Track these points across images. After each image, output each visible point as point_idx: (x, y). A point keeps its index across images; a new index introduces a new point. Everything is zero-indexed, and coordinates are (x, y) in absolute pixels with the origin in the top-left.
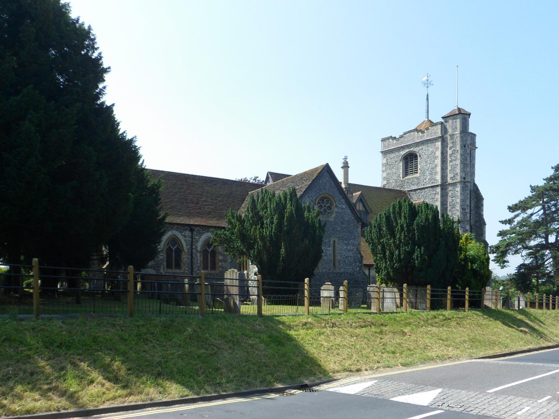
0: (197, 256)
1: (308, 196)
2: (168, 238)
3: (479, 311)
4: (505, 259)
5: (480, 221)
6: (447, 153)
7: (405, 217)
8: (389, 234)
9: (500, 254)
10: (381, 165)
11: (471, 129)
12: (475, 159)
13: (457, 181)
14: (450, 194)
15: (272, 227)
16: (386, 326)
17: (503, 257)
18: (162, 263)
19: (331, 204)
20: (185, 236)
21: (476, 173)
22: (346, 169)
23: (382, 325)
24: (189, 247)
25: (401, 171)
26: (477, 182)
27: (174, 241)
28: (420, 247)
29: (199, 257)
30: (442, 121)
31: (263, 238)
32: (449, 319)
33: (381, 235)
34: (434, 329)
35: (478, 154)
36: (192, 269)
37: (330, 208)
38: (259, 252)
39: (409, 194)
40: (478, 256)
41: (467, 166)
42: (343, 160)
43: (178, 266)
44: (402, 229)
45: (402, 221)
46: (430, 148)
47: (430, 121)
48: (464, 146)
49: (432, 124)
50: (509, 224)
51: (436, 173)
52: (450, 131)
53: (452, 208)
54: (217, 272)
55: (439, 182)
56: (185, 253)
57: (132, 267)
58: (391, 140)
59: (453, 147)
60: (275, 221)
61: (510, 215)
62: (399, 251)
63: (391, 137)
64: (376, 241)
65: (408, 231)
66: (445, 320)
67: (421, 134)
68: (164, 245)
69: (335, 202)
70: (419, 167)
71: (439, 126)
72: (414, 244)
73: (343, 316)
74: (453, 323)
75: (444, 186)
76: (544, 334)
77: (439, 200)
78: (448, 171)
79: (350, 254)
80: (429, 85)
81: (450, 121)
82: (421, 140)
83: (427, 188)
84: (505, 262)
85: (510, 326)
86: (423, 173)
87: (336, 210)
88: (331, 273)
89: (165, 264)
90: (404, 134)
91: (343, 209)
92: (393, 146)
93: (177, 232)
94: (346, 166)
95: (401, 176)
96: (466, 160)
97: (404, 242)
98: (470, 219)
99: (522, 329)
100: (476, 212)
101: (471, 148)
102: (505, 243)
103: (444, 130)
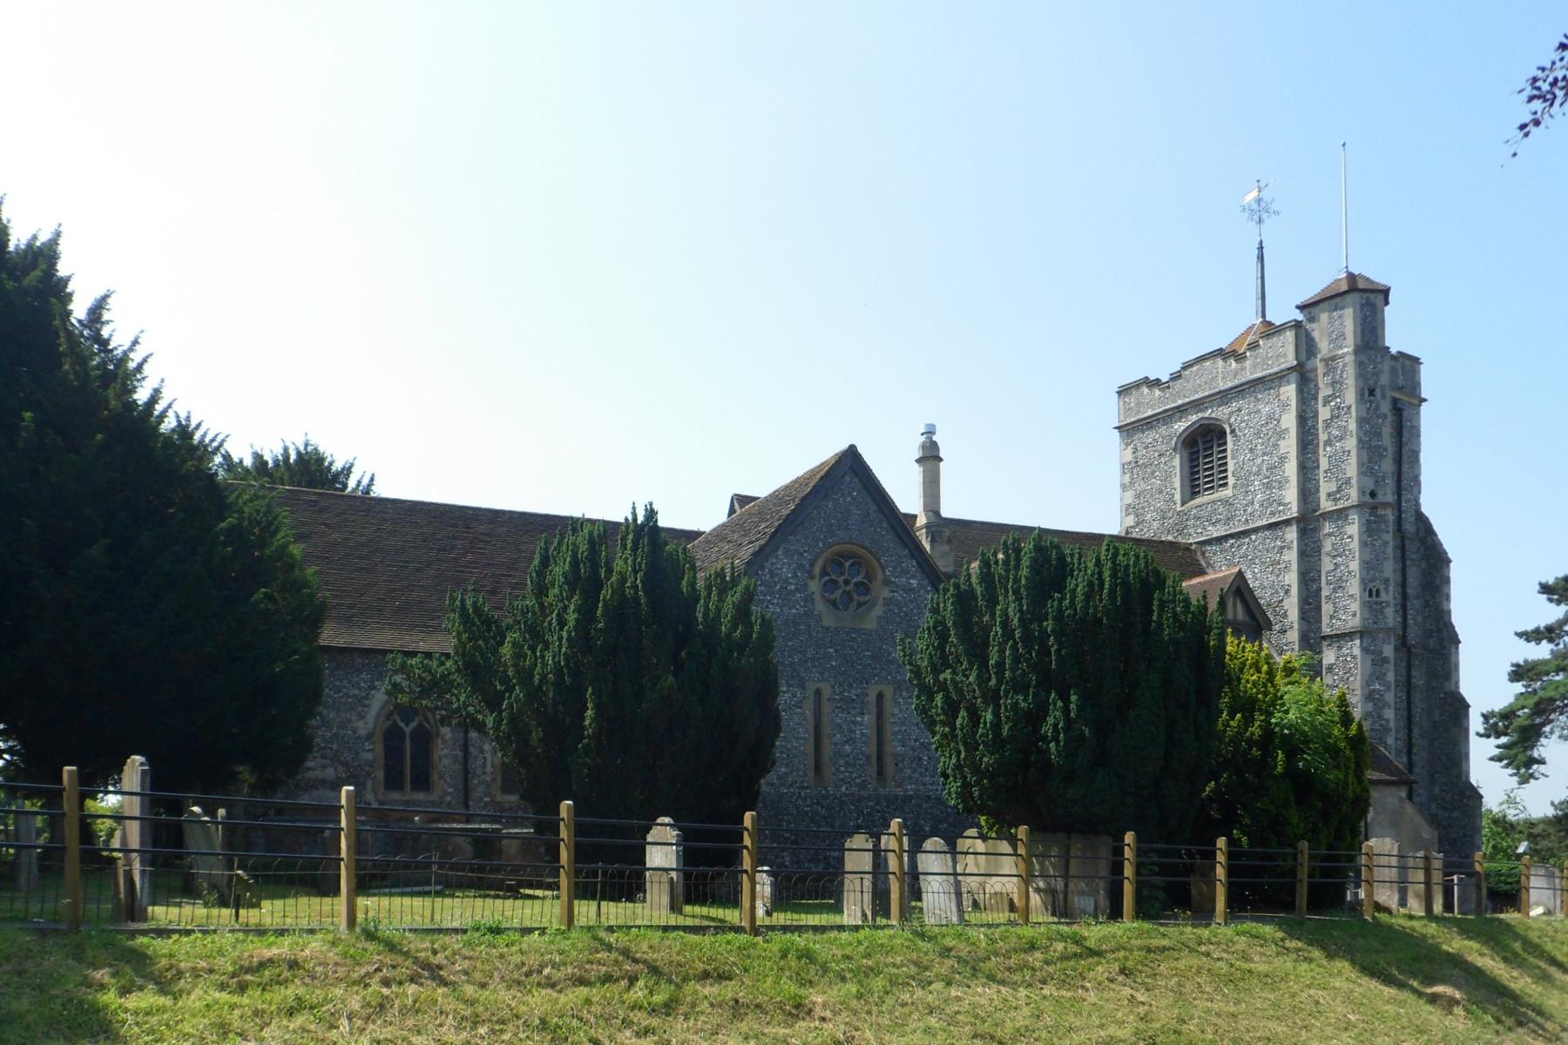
0: (482, 751)
1: (786, 553)
4: (1536, 754)
5: (1439, 631)
6: (1316, 415)
7: (1016, 592)
8: (967, 652)
9: (1515, 737)
10: (1117, 469)
11: (1395, 340)
12: (1418, 436)
13: (1347, 504)
14: (1327, 546)
16: (723, 977)
17: (1526, 749)
18: (369, 774)
19: (868, 576)
21: (1422, 478)
22: (930, 464)
23: (705, 975)
25: (1177, 482)
26: (1426, 509)
28: (1065, 697)
29: (488, 756)
30: (1300, 316)
31: (525, 676)
32: (1098, 953)
33: (944, 657)
37: (864, 588)
38: (513, 720)
39: (1203, 554)
40: (1314, 727)
41: (1382, 456)
42: (923, 438)
43: (422, 781)
44: (1008, 633)
45: (1010, 608)
47: (1270, 324)
48: (1368, 392)
49: (1270, 330)
50: (1551, 640)
52: (1324, 347)
55: (1294, 511)
56: (444, 741)
58: (1145, 390)
60: (572, 617)
62: (996, 714)
63: (1147, 382)
65: (1027, 638)
69: (883, 569)
70: (1231, 467)
71: (1290, 336)
72: (1047, 681)
75: (1309, 522)
76: (1540, 1013)
77: (1295, 566)
78: (1322, 475)
80: (1264, 216)
81: (1324, 317)
82: (1236, 382)
83: (1255, 530)
84: (1534, 761)
85: (1389, 980)
86: (1244, 484)
87: (886, 593)
88: (869, 798)
89: (380, 774)
91: (910, 590)
92: (1151, 407)
94: (930, 456)
95: (1178, 497)
96: (1379, 435)
99: (1439, 989)
100: (1427, 605)
101: (1395, 401)
102: (1531, 701)
103: (1306, 345)
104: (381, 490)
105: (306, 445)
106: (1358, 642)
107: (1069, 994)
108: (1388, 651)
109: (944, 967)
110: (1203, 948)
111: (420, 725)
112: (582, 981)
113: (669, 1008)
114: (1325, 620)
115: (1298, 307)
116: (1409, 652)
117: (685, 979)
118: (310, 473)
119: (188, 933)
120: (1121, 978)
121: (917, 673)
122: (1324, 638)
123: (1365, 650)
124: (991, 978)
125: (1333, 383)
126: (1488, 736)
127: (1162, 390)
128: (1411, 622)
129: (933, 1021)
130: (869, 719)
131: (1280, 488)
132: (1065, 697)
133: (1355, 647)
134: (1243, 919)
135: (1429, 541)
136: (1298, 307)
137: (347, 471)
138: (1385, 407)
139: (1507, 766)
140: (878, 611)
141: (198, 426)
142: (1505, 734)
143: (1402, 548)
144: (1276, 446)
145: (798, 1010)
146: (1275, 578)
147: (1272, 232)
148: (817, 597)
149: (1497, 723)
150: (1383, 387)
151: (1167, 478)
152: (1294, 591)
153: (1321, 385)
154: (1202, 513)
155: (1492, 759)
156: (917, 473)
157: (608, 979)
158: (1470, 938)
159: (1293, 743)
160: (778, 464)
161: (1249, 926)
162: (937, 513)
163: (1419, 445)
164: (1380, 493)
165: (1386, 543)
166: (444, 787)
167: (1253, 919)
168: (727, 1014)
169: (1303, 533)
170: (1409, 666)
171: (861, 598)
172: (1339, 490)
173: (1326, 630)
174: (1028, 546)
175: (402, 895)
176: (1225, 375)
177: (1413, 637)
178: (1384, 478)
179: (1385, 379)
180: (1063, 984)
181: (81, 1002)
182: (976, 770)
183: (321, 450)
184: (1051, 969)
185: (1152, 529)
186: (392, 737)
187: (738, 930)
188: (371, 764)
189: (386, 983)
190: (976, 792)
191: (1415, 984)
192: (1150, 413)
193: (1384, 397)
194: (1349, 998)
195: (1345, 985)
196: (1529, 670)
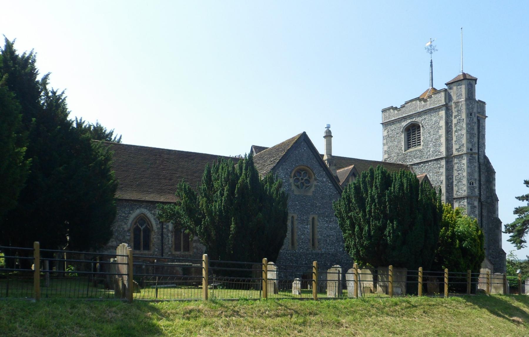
0: (168, 236)
2: (136, 217)
3: (462, 297)
4: (523, 239)
5: (492, 196)
7: (376, 186)
8: (358, 206)
9: (516, 233)
10: (382, 138)
11: (478, 96)
12: (485, 129)
13: (462, 153)
14: (456, 167)
15: (222, 200)
16: (316, 314)
19: (309, 177)
20: (154, 214)
22: (328, 138)
23: (310, 314)
24: (159, 226)
25: (403, 144)
26: (487, 154)
27: (142, 219)
28: (392, 222)
29: (170, 238)
30: (446, 87)
31: (210, 213)
32: (416, 307)
34: (389, 320)
36: (162, 250)
37: (308, 181)
38: (206, 229)
39: (412, 168)
40: (468, 232)
42: (326, 129)
43: (147, 247)
45: (374, 192)
46: (434, 118)
47: (435, 89)
48: (470, 114)
49: (435, 91)
51: (440, 145)
52: (455, 98)
53: (458, 183)
54: (191, 253)
55: (444, 154)
56: (155, 232)
57: (38, 242)
58: (392, 111)
59: (458, 115)
60: (225, 193)
62: (369, 227)
63: (392, 108)
64: (344, 215)
65: (380, 203)
66: (409, 307)
67: (423, 103)
68: (131, 224)
69: (314, 174)
70: (422, 138)
71: (443, 94)
72: (386, 217)
73: (258, 302)
74: (418, 312)
75: (449, 159)
77: (444, 174)
78: (454, 142)
79: (333, 232)
80: (433, 51)
81: (455, 88)
82: (424, 109)
83: (431, 161)
85: (499, 315)
86: (426, 145)
87: (315, 183)
88: (309, 254)
90: (406, 104)
91: (323, 182)
93: (146, 210)
94: (328, 136)
95: (403, 148)
96: (473, 129)
98: (480, 194)
99: (515, 318)
100: (487, 187)
101: (478, 117)
102: (522, 221)
104: (124, 142)
105: (97, 124)
106: (466, 200)
107: (410, 319)
108: (476, 203)
109: (374, 311)
110: (444, 305)
111: (146, 227)
112: (277, 316)
113: (304, 323)
114: (455, 192)
115: (446, 84)
116: (482, 204)
117: (305, 315)
118: (98, 132)
119: (238, 300)
120: (424, 314)
121: (340, 213)
122: (454, 199)
123: (468, 203)
124: (388, 314)
125: (458, 111)
126: (506, 233)
127: (398, 111)
128: (482, 193)
129: (376, 327)
130: (309, 226)
131: (439, 147)
132: (392, 222)
133: (465, 202)
134: (452, 295)
135: (488, 166)
136: (446, 84)
137: (111, 134)
138: (475, 120)
139: (513, 243)
141: (84, 122)
142: (512, 232)
143: (479, 168)
145: (339, 325)
146: (437, 177)
147: (435, 57)
148: (293, 185)
149: (511, 228)
150: (475, 113)
151: (399, 142)
152: (444, 182)
153: (454, 111)
154: (412, 155)
155: (508, 241)
156: (324, 141)
157: (284, 315)
158: (520, 302)
159: (462, 238)
160: (274, 136)
162: (331, 155)
163: (485, 132)
165: (475, 166)
166: (155, 249)
167: (456, 295)
168: (321, 326)
169: (447, 162)
170: (482, 209)
171: (307, 185)
172: (460, 148)
173: (455, 196)
174: (377, 173)
175: (165, 288)
176: (420, 107)
177: (483, 199)
178: (475, 144)
179: (475, 110)
180: (408, 316)
181: (148, 323)
182: (362, 246)
183: (102, 126)
184: (403, 311)
186: (137, 231)
187: (312, 299)
189: (226, 316)
190: (361, 253)
191: (507, 316)
192: (393, 119)
193: (475, 116)
194: (489, 321)
195: (487, 316)
196: (521, 210)
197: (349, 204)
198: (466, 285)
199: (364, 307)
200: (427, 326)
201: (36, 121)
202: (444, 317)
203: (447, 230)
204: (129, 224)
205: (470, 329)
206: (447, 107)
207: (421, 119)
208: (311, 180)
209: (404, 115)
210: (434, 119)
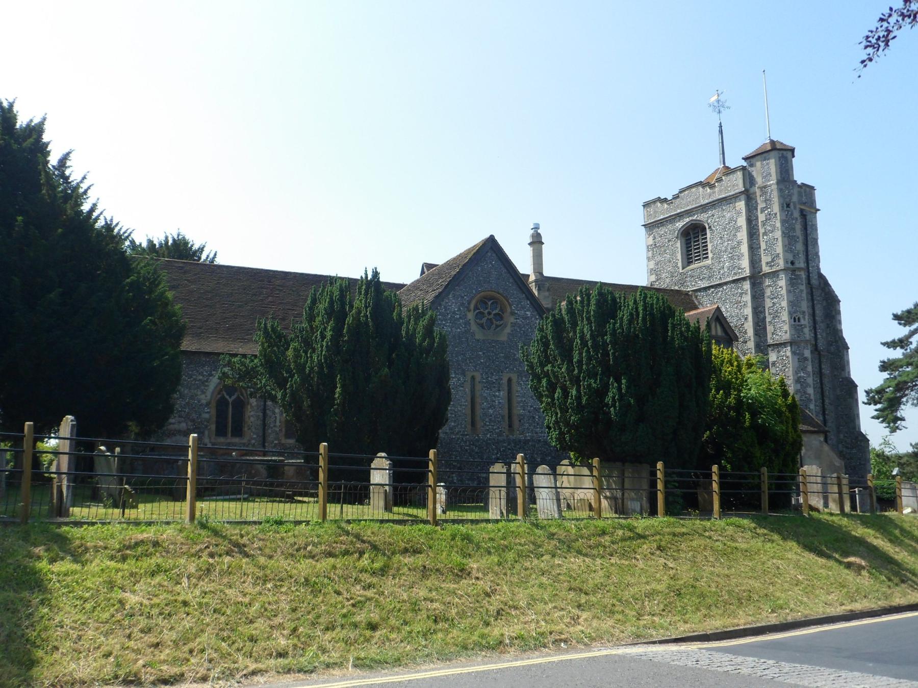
0: (274, 413)
4: (899, 415)
5: (836, 342)
6: (757, 218)
7: (588, 319)
8: (560, 354)
9: (886, 404)
11: (800, 175)
12: (816, 230)
13: (778, 269)
14: (768, 292)
16: (417, 552)
17: (893, 412)
18: (206, 427)
19: (501, 310)
21: (820, 254)
22: (536, 246)
23: (405, 551)
25: (679, 256)
26: (823, 271)
29: (278, 416)
30: (745, 164)
31: (301, 368)
33: (547, 357)
34: (576, 563)
35: (823, 222)
37: (500, 317)
38: (293, 395)
39: (696, 297)
42: (532, 231)
43: (238, 431)
44: (584, 343)
47: (728, 168)
48: (786, 206)
49: (728, 171)
50: (902, 347)
51: (740, 257)
52: (759, 180)
55: (747, 272)
56: (252, 407)
58: (659, 205)
59: (766, 208)
60: (329, 334)
61: (901, 331)
62: (578, 391)
65: (595, 346)
68: (213, 393)
69: (510, 305)
70: (710, 247)
71: (739, 174)
72: (608, 371)
74: (646, 547)
75: (756, 278)
77: (749, 304)
78: (762, 252)
80: (722, 109)
81: (758, 164)
82: (711, 200)
83: (726, 283)
84: (897, 419)
85: (821, 554)
87: (512, 320)
88: (504, 441)
89: (213, 427)
90: (680, 192)
91: (526, 318)
92: (663, 214)
94: (537, 241)
95: (680, 265)
96: (794, 229)
97: (588, 370)
99: (852, 559)
100: (828, 326)
101: (802, 211)
103: (749, 180)
104: (219, 261)
105: (178, 235)
107: (627, 563)
108: (807, 353)
109: (550, 545)
110: (707, 534)
111: (238, 397)
112: (330, 554)
113: (383, 571)
114: (769, 336)
116: (819, 354)
117: (393, 553)
118: (180, 250)
119: (93, 524)
120: (658, 552)
121: (531, 366)
122: (769, 346)
123: (793, 353)
124: (579, 552)
125: (766, 201)
126: (870, 404)
127: (669, 204)
128: (819, 336)
129: (544, 580)
130: (503, 394)
131: (739, 259)
133: (788, 351)
137: (201, 250)
138: (796, 214)
139: (882, 422)
140: (508, 330)
142: (880, 403)
144: (735, 235)
145: (462, 572)
146: (739, 311)
147: (726, 118)
148: (472, 322)
149: (874, 396)
150: (794, 203)
151: (673, 253)
155: (873, 418)
156: (529, 251)
157: (346, 553)
158: (868, 527)
159: (755, 408)
161: (734, 519)
162: (541, 274)
164: (796, 262)
165: (802, 291)
167: (736, 516)
168: (419, 575)
169: (753, 285)
171: (498, 323)
172: (773, 261)
173: (770, 342)
174: (594, 293)
175: (224, 500)
176: (704, 196)
177: (821, 345)
178: (798, 254)
179: (795, 198)
180: (623, 556)
182: (567, 424)
184: (615, 547)
185: (665, 283)
186: (221, 405)
187: (425, 522)
188: (208, 421)
189: (212, 555)
190: (567, 437)
191: (837, 556)
193: (795, 208)
194: (797, 566)
195: (794, 557)
196: (891, 365)
197: (545, 351)
198: (760, 495)
199: (532, 538)
200: (658, 575)
201: (23, 221)
202: (699, 558)
203: (727, 395)
204: (209, 394)
205: (750, 582)
206: (748, 196)
207: (706, 216)
208: (506, 315)
209: (679, 211)
210: (728, 215)
